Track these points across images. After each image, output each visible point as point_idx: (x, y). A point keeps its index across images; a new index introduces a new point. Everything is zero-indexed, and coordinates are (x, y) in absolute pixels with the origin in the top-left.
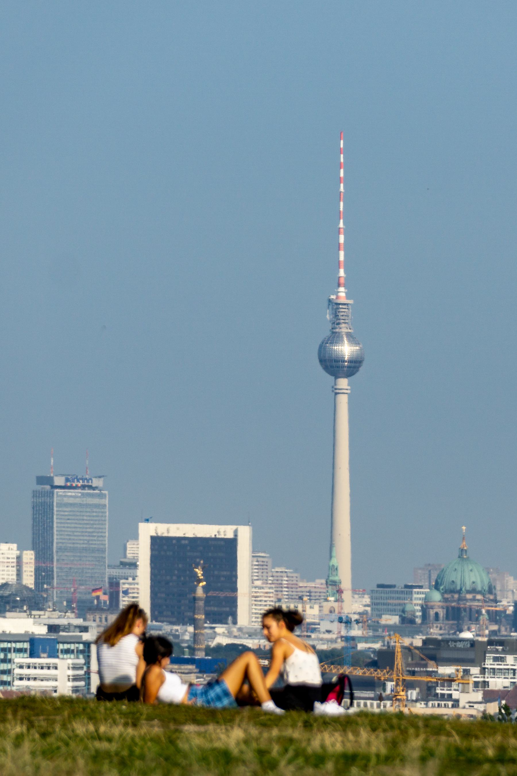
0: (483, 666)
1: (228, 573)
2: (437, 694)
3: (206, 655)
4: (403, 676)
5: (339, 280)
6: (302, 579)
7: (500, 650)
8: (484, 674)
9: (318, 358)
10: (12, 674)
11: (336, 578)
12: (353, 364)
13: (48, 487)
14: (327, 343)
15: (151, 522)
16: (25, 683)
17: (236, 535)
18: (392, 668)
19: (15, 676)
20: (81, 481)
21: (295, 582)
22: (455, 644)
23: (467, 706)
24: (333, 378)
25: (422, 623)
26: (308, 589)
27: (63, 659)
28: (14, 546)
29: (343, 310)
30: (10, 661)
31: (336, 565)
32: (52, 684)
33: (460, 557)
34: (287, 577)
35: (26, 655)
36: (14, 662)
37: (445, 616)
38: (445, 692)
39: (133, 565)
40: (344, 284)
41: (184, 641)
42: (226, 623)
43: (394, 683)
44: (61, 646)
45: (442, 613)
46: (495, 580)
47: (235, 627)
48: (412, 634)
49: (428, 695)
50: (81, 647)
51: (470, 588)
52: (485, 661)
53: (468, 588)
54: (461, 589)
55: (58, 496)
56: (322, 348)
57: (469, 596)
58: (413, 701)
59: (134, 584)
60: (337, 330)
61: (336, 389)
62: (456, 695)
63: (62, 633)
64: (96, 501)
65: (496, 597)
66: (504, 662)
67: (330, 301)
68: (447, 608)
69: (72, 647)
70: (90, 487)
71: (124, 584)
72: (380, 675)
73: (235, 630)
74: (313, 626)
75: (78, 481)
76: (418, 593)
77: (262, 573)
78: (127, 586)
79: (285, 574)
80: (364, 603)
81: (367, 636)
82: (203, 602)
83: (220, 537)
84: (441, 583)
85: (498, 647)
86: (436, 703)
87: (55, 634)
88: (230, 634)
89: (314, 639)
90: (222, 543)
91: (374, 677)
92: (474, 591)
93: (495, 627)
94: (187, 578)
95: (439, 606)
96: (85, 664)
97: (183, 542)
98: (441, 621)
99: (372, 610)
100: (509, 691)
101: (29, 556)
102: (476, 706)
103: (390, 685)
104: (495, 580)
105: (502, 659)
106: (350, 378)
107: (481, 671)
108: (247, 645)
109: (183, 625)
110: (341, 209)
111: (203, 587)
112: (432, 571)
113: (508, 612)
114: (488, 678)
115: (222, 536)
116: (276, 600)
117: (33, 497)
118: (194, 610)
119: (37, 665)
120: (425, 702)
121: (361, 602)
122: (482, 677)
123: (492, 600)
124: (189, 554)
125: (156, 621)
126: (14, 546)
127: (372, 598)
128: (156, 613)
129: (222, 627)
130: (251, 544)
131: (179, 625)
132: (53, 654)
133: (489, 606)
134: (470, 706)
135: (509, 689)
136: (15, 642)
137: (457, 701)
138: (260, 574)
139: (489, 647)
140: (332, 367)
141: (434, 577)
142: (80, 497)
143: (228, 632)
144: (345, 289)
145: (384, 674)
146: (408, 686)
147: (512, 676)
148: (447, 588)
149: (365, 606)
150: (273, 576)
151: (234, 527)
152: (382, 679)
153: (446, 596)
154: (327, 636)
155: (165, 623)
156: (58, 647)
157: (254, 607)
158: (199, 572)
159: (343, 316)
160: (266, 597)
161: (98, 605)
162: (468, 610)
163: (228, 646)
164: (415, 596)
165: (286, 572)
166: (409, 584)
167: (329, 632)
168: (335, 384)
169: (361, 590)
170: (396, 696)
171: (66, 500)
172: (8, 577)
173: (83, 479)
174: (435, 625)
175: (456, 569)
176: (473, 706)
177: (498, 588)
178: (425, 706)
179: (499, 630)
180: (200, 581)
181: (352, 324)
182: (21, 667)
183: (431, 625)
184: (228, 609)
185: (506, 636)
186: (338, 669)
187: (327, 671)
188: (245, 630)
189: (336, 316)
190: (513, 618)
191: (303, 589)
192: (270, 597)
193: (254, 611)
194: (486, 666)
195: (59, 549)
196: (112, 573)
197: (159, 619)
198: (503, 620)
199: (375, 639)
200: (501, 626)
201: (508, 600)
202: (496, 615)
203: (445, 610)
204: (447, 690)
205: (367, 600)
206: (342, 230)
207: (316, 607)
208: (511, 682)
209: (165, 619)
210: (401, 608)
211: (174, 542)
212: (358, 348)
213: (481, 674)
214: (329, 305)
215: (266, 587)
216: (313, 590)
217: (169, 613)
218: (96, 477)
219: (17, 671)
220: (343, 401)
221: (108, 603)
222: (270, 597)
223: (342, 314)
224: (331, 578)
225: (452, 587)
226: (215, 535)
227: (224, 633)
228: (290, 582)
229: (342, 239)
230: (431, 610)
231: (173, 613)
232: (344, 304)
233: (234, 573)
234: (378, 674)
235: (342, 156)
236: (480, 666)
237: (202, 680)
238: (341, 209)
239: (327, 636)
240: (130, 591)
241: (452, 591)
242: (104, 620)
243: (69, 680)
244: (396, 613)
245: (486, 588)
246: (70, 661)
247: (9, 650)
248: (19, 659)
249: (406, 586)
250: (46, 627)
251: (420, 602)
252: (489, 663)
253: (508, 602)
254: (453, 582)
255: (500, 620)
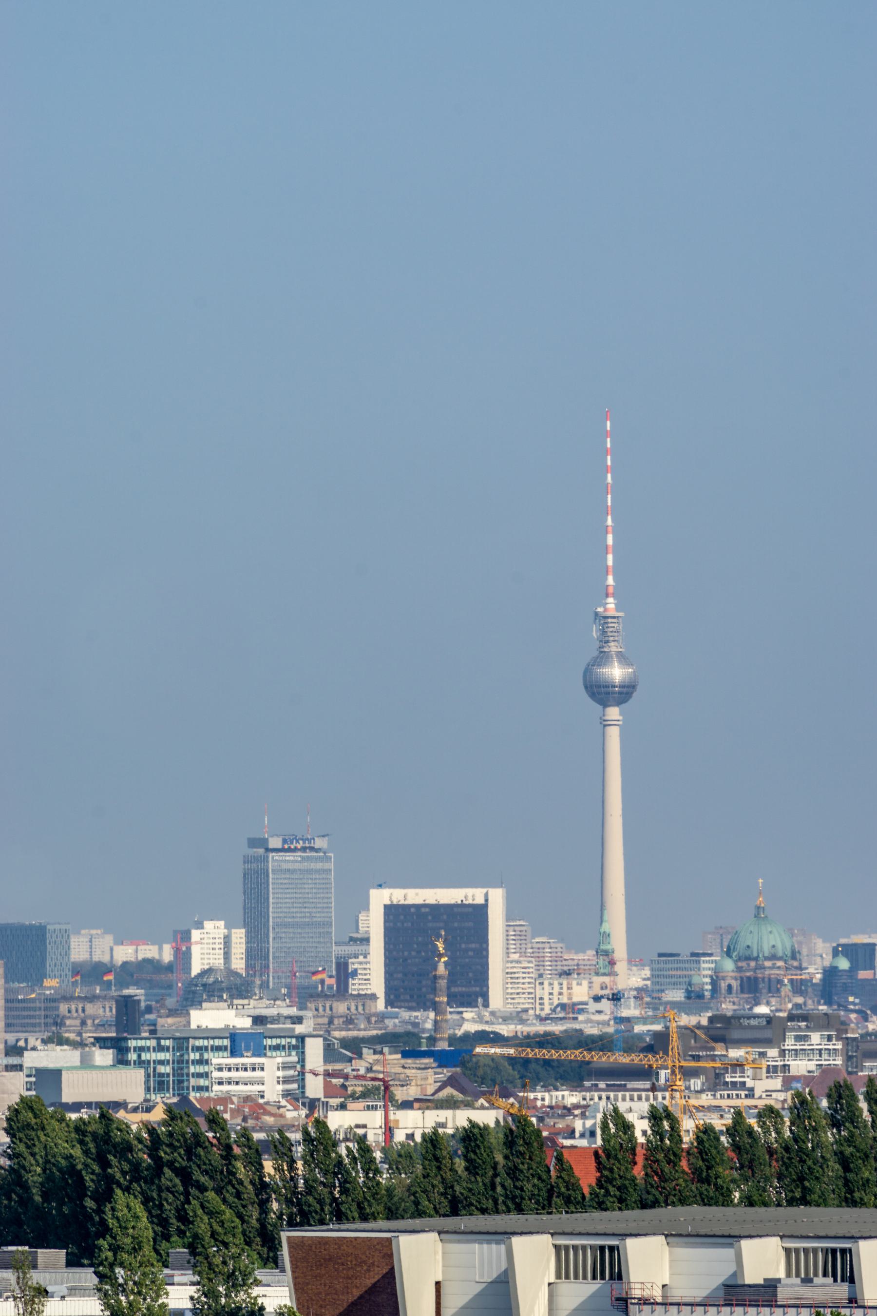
0: (783, 1048)
1: (478, 946)
2: (727, 1082)
3: (449, 1046)
4: (680, 1062)
5: (607, 590)
6: (569, 949)
7: (803, 1027)
8: (785, 1056)
9: (582, 684)
10: (210, 1079)
11: (608, 947)
12: (625, 690)
13: (261, 851)
14: (594, 665)
15: (385, 888)
16: (225, 1088)
17: (487, 900)
18: (666, 1053)
19: (214, 1080)
20: (301, 842)
21: (559, 954)
22: (748, 1021)
23: (764, 1095)
24: (601, 707)
25: (712, 997)
26: (576, 962)
27: (271, 1057)
28: (221, 924)
29: (613, 625)
30: (207, 1062)
31: (607, 931)
32: (258, 1088)
33: (757, 916)
34: (551, 948)
35: (225, 1054)
36: (211, 1064)
37: (739, 988)
38: (738, 1079)
39: (366, 940)
40: (613, 594)
41: (424, 1031)
42: (477, 1007)
43: (669, 1071)
44: (269, 1042)
45: (735, 984)
46: (800, 943)
47: (487, 1011)
48: (698, 1012)
49: (716, 1085)
50: (294, 1041)
51: (770, 953)
52: (785, 1041)
53: (766, 955)
54: (758, 956)
55: (273, 860)
56: (588, 672)
57: (768, 964)
58: (697, 1092)
59: (366, 963)
60: (606, 650)
61: (605, 720)
62: (750, 1083)
63: (269, 1026)
64: (319, 866)
65: (801, 964)
66: (807, 1041)
67: (596, 614)
68: (742, 978)
69: (283, 1042)
70: (312, 849)
71: (353, 963)
72: (651, 1062)
73: (487, 1014)
74: (580, 1007)
75: (297, 842)
76: (707, 962)
77: (520, 944)
78: (356, 966)
79: (547, 945)
80: (644, 976)
81: (645, 1016)
82: (446, 981)
83: (467, 902)
84: (734, 948)
85: (800, 1024)
86: (726, 1093)
87: (261, 1027)
88: (480, 1019)
89: (582, 1022)
90: (470, 910)
91: (645, 1064)
92: (773, 957)
93: (800, 1000)
94: (430, 953)
95: (731, 977)
96: (298, 1062)
97: (423, 910)
98: (734, 995)
99: (652, 983)
100: (814, 1077)
101: (239, 936)
102: (774, 1095)
103: (663, 1074)
104: (800, 943)
105: (805, 1038)
106: (623, 705)
107: (779, 1052)
108: (501, 1032)
109: (425, 1010)
110: (609, 504)
111: (444, 962)
112: (724, 936)
113: (814, 981)
114: (788, 1060)
115: (470, 901)
116: (537, 976)
117: (244, 863)
118: (434, 990)
119: (240, 1066)
120: (713, 1093)
121: (640, 975)
122: (781, 1061)
123: (796, 968)
124: (430, 925)
125: (392, 1008)
126: (221, 924)
127: (652, 970)
128: (392, 997)
129: (472, 1012)
130: (505, 909)
131: (419, 1010)
132: (260, 1051)
133: (792, 975)
134: (767, 1096)
135: (815, 1074)
136: (213, 1038)
137: (752, 1090)
138: (518, 946)
139: (789, 1024)
140: (599, 693)
141: (726, 944)
142: (300, 862)
143: (479, 1017)
144: (614, 600)
145: (657, 1060)
146: (689, 1074)
147: (819, 1058)
148: (741, 955)
149: (644, 979)
150: (532, 948)
151: (485, 890)
152: (655, 1066)
153: (740, 964)
154: (598, 1017)
155: (403, 1009)
156: (265, 1044)
157: (509, 986)
158: (440, 946)
159: (612, 632)
160: (524, 973)
161: (322, 991)
162: (766, 980)
163: (478, 1033)
164: (703, 965)
165: (549, 943)
166: (696, 951)
167: (599, 1012)
168: (604, 715)
169: (637, 960)
170: (672, 1086)
171: (285, 866)
172: (214, 961)
173: (304, 841)
174: (728, 1000)
175: (751, 932)
176: (771, 1096)
177: (805, 951)
178: (712, 1097)
179: (805, 1004)
180: (440, 956)
181: (622, 643)
182: (220, 1069)
183: (723, 1000)
184: (478, 989)
185: (813, 1010)
186: (608, 1057)
187: (595, 1059)
188: (498, 1014)
189: (604, 632)
190: (821, 988)
191: (570, 962)
192: (529, 973)
193: (510, 991)
194: (786, 1047)
195: (277, 925)
196: (340, 952)
197: (396, 1004)
198: (810, 990)
199: (654, 1020)
200: (807, 999)
201: (816, 967)
202: (801, 984)
203: (739, 982)
204: (740, 1077)
205: (647, 972)
206: (610, 529)
207: (585, 983)
208: (817, 1065)
209: (403, 1004)
210: (687, 980)
211: (413, 910)
212: (630, 670)
213: (780, 1056)
214: (596, 619)
215: (525, 961)
216: (581, 962)
217: (408, 997)
218: (318, 837)
219: (216, 1074)
220: (614, 735)
221: (335, 988)
222: (529, 973)
223: (611, 629)
224: (603, 947)
225: (747, 953)
226: (462, 901)
227: (473, 1018)
228: (554, 955)
229: (610, 540)
230: (722, 981)
231: (412, 997)
232: (614, 617)
233: (484, 946)
234: (649, 1060)
235: (609, 440)
236: (779, 1047)
237: (443, 1075)
238: (609, 504)
239: (598, 1017)
240: (359, 972)
241: (748, 958)
242: (328, 1008)
243: (278, 1082)
244: (682, 987)
245: (789, 953)
246: (279, 1060)
247: (206, 1048)
248: (217, 1059)
249: (693, 954)
250: (250, 1020)
251: (710, 972)
252: (790, 1043)
253: (817, 969)
254: (748, 947)
255: (806, 990)
